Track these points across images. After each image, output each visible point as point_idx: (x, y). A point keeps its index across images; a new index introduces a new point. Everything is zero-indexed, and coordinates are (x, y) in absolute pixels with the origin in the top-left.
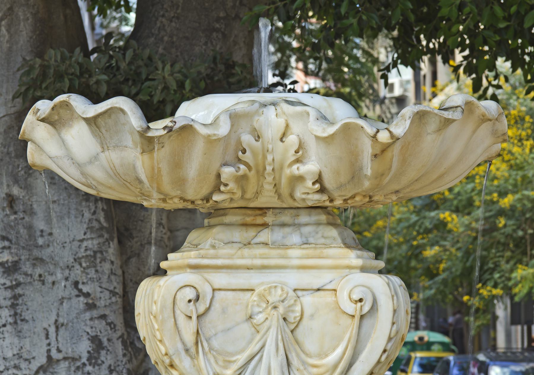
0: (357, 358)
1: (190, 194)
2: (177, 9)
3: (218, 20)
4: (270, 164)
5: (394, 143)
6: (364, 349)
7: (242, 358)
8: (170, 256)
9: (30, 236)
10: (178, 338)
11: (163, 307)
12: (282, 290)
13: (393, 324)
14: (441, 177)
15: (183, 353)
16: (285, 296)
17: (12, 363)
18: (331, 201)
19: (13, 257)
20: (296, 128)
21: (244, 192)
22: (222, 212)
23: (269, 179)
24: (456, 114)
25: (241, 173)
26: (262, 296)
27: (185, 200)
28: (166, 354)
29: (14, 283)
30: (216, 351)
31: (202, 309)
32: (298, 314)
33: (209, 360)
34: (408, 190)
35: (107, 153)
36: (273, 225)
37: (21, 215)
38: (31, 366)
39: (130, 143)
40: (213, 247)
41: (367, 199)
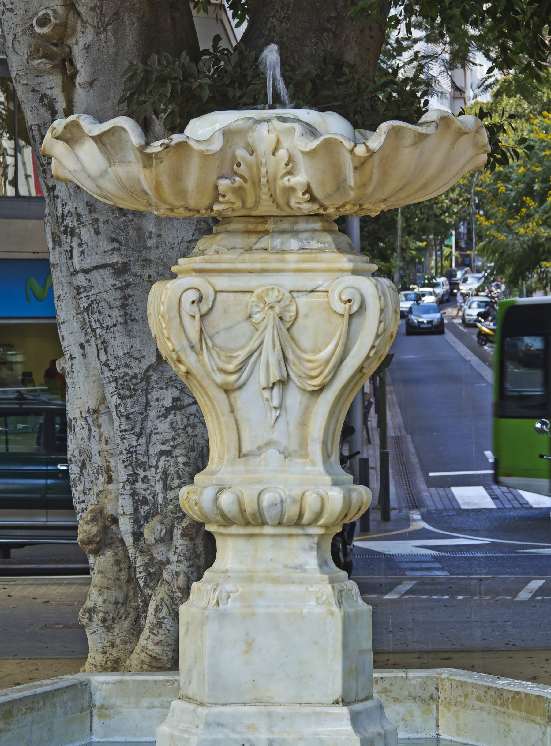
0: (348, 354)
1: (192, 203)
2: (288, 9)
3: (329, 19)
4: (264, 177)
5: (370, 156)
6: (354, 345)
7: (242, 354)
8: (181, 261)
9: (139, 238)
10: (184, 336)
11: (169, 308)
12: (279, 291)
13: (380, 322)
14: (424, 186)
15: (188, 350)
16: (281, 297)
17: (123, 362)
18: (325, 209)
19: (122, 259)
20: (286, 143)
21: (244, 202)
22: (228, 220)
23: (265, 190)
24: (429, 128)
25: (236, 185)
26: (260, 298)
27: (190, 210)
28: (174, 350)
29: (124, 284)
30: (219, 347)
31: (204, 308)
32: (293, 314)
33: (211, 355)
34: (394, 199)
35: (113, 168)
36: (273, 232)
37: (131, 218)
38: (141, 365)
39: (133, 159)
40: (217, 252)
41: (357, 208)
